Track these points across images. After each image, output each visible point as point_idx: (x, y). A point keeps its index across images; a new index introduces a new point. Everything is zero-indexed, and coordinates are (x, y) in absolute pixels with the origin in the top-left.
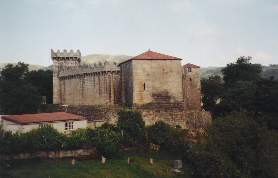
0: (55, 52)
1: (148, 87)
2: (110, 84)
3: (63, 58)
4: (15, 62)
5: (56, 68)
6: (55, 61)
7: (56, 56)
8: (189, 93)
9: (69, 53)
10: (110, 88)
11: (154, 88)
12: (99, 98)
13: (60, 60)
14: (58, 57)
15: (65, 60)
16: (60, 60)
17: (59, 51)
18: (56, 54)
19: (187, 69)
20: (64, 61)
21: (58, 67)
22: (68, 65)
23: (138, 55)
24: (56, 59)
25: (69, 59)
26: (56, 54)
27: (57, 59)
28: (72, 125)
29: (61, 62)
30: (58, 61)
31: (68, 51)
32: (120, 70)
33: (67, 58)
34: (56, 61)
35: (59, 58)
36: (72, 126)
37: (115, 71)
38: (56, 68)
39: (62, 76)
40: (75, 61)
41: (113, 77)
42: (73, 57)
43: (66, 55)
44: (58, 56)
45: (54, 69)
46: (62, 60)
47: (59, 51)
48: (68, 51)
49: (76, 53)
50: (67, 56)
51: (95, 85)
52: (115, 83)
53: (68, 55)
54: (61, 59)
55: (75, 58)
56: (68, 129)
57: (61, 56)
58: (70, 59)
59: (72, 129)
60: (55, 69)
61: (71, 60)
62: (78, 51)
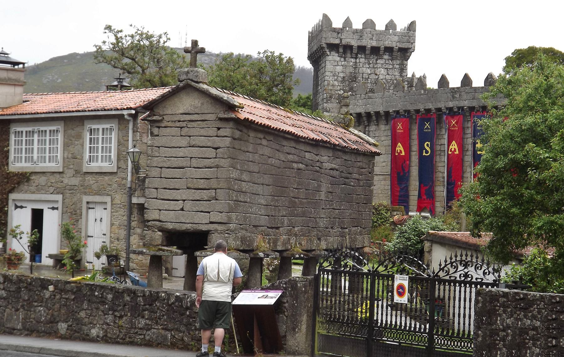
0: (334, 26)
3: (362, 49)
4: (524, 46)
5: (336, 83)
7: (337, 41)
13: (349, 55)
14: (344, 42)
15: (365, 55)
16: (349, 55)
17: (348, 22)
18: (338, 31)
20: (362, 60)
21: (344, 77)
22: (378, 72)
23: (52, 60)
24: (338, 52)
25: (381, 52)
26: (338, 33)
27: (341, 50)
29: (353, 60)
30: (341, 57)
31: (380, 26)
33: (375, 51)
34: (338, 59)
35: (348, 48)
39: (359, 110)
40: (398, 62)
42: (394, 45)
44: (348, 40)
45: (328, 85)
47: (348, 22)
48: (380, 26)
49: (381, 33)
50: (374, 44)
54: (355, 51)
56: (97, 161)
57: (354, 43)
58: (384, 54)
61: (386, 57)
62: (412, 27)
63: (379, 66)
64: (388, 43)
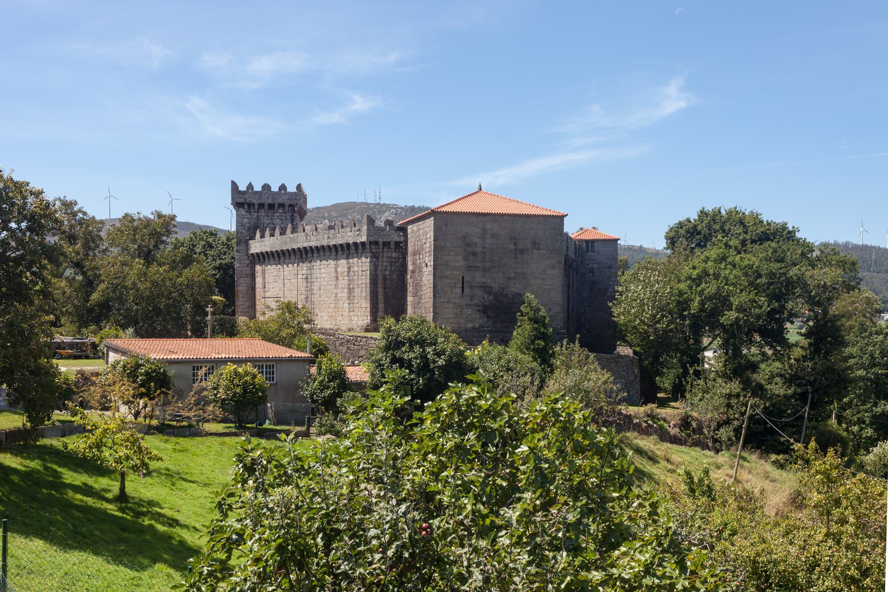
1: (471, 287)
2: (377, 275)
3: (261, 206)
5: (244, 231)
6: (243, 212)
7: (243, 201)
8: (584, 309)
9: (275, 193)
10: (377, 287)
11: (487, 289)
12: (347, 310)
16: (253, 210)
19: (584, 243)
20: (263, 214)
24: (244, 208)
27: (246, 207)
28: (273, 372)
32: (402, 239)
33: (271, 206)
35: (250, 205)
36: (273, 374)
37: (386, 244)
38: (244, 231)
41: (382, 257)
43: (268, 198)
46: (258, 209)
50: (270, 201)
51: (337, 277)
52: (387, 273)
53: (273, 199)
54: (257, 206)
55: (290, 205)
59: (273, 380)
60: (242, 233)
61: (280, 211)
63: (275, 217)
64: (280, 201)
